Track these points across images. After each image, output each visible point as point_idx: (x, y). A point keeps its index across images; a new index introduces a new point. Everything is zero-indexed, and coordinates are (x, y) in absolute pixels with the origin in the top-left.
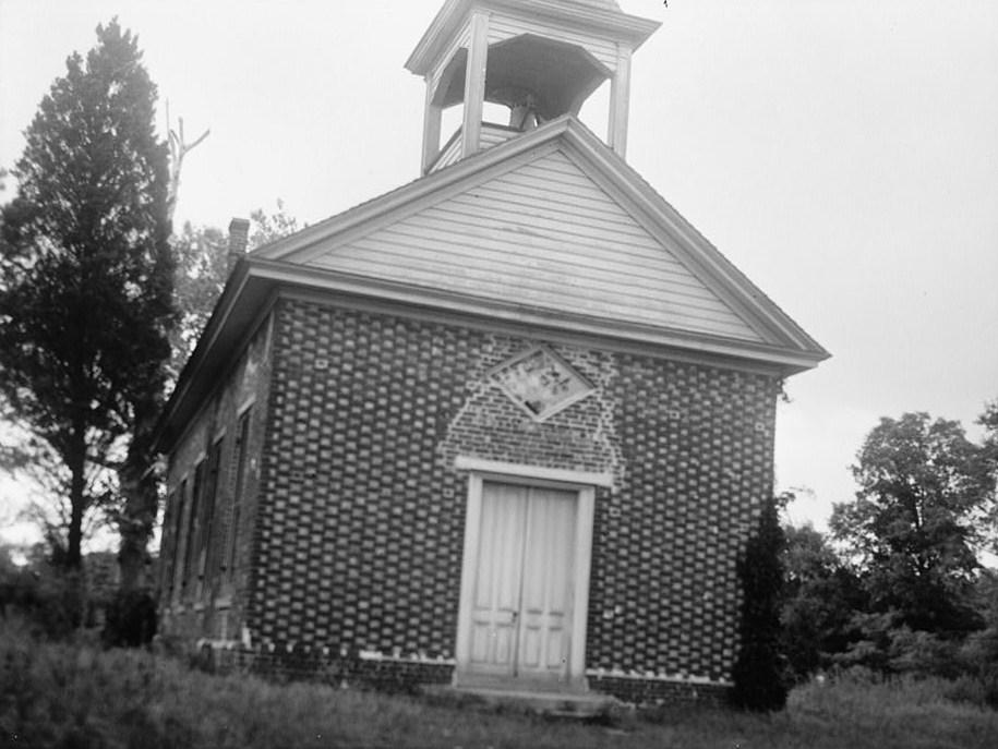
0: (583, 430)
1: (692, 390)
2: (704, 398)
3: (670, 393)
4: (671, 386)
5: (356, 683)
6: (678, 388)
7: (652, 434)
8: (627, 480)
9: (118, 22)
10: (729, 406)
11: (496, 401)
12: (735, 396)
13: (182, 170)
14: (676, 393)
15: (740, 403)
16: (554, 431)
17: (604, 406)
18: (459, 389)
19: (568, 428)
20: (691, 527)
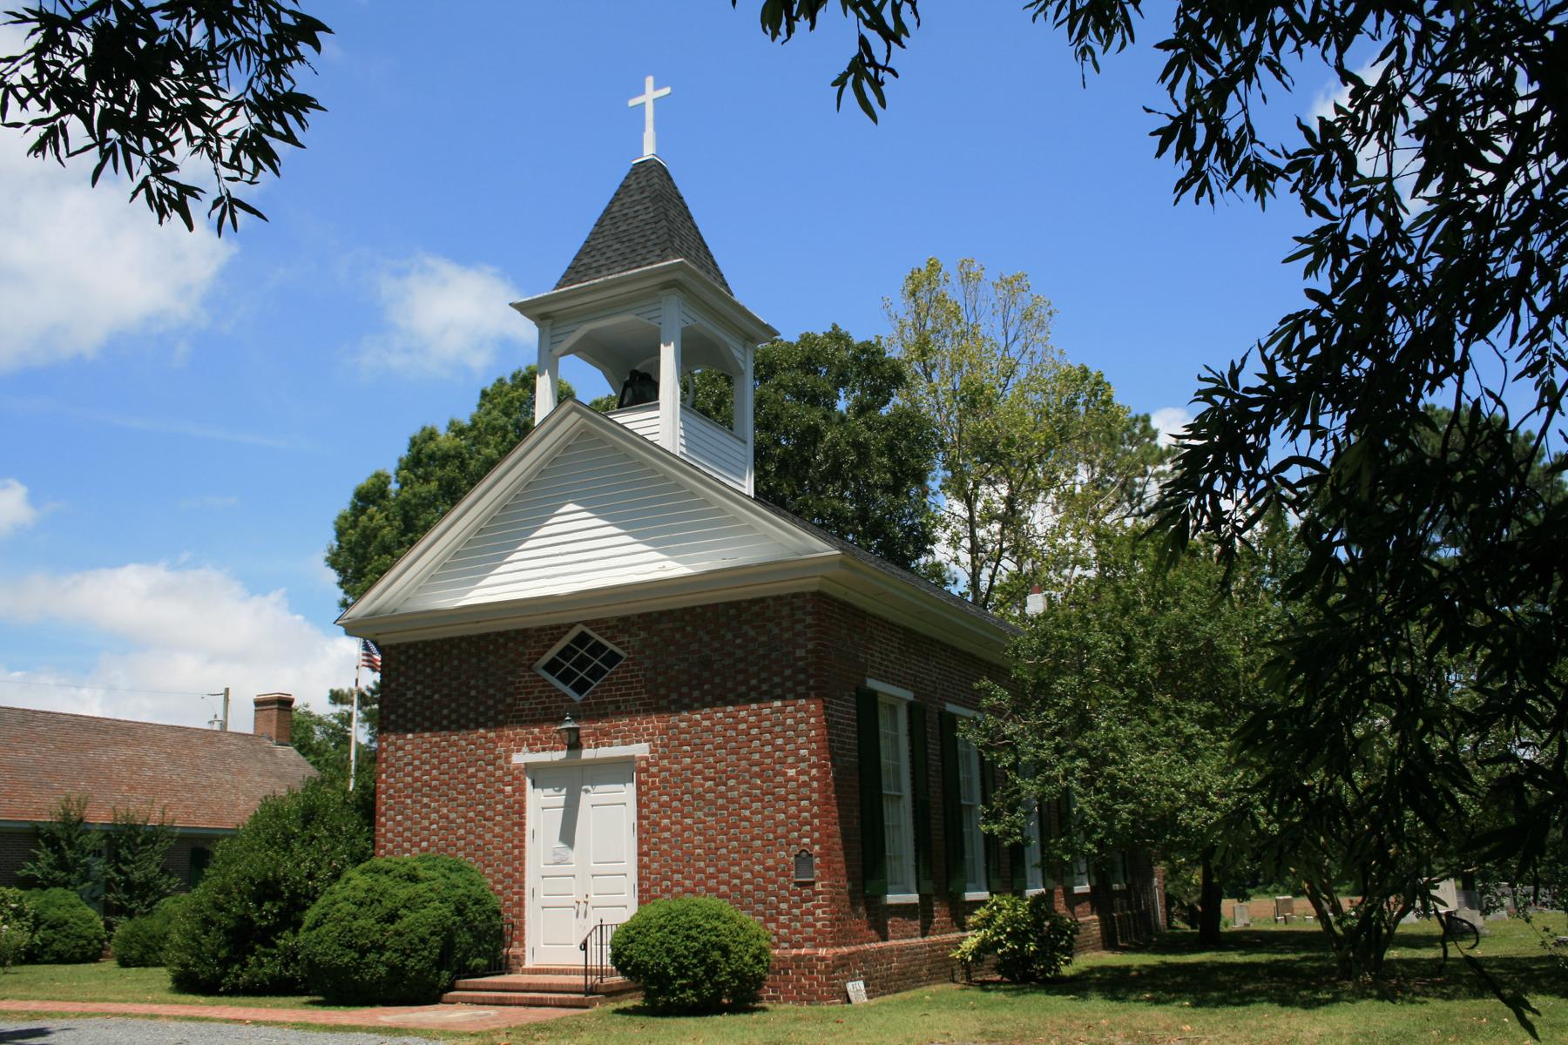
0: (618, 701)
1: (746, 628)
2: (736, 637)
3: (700, 641)
4: (701, 633)
5: (518, 951)
6: (708, 633)
7: (685, 690)
8: (663, 746)
9: (340, 594)
10: (764, 639)
11: (540, 692)
12: (770, 625)
13: (156, 4)
14: (706, 638)
15: (776, 631)
16: (591, 710)
17: (1137, 640)
18: (511, 689)
19: (604, 703)
20: (732, 782)
